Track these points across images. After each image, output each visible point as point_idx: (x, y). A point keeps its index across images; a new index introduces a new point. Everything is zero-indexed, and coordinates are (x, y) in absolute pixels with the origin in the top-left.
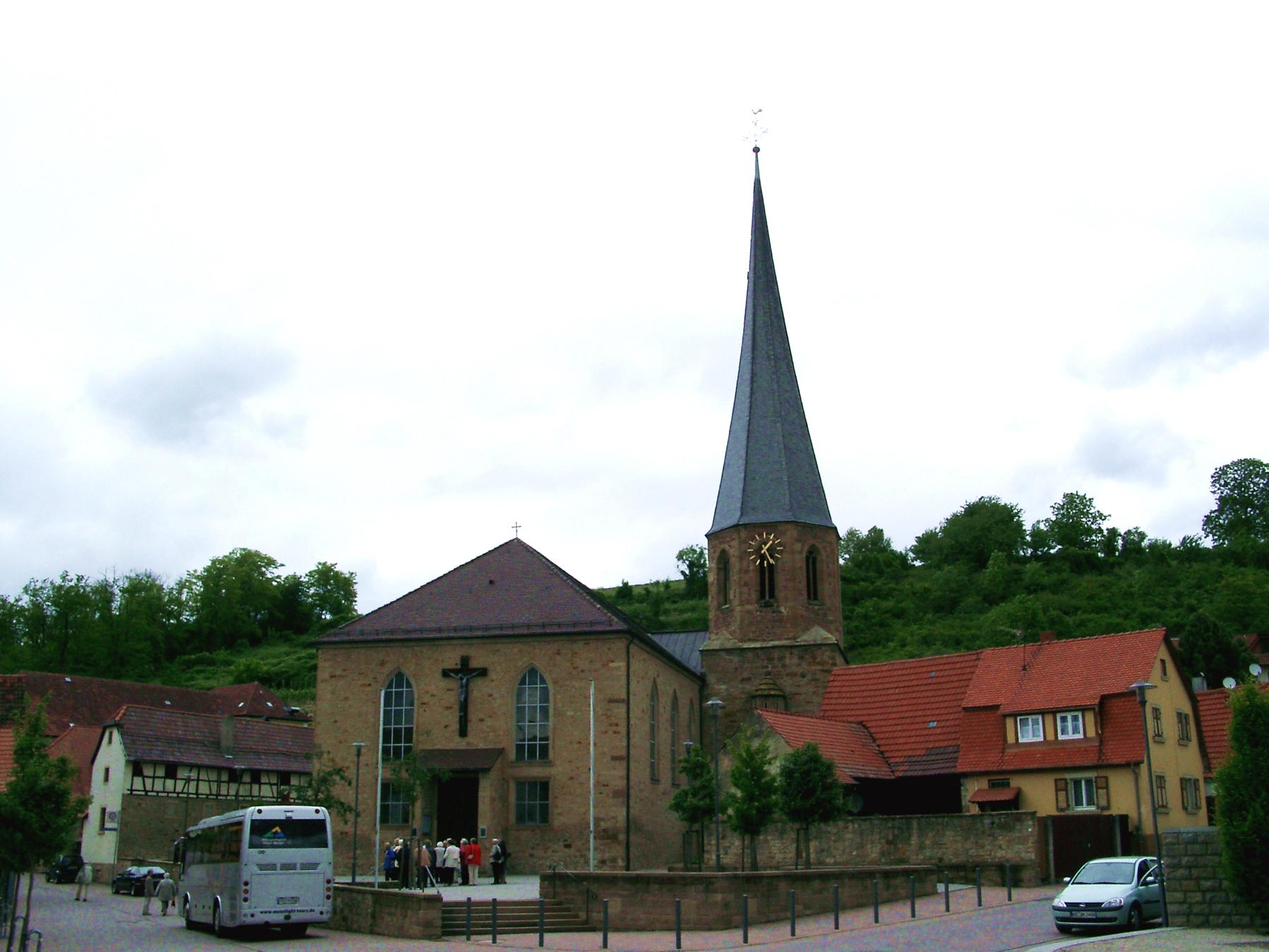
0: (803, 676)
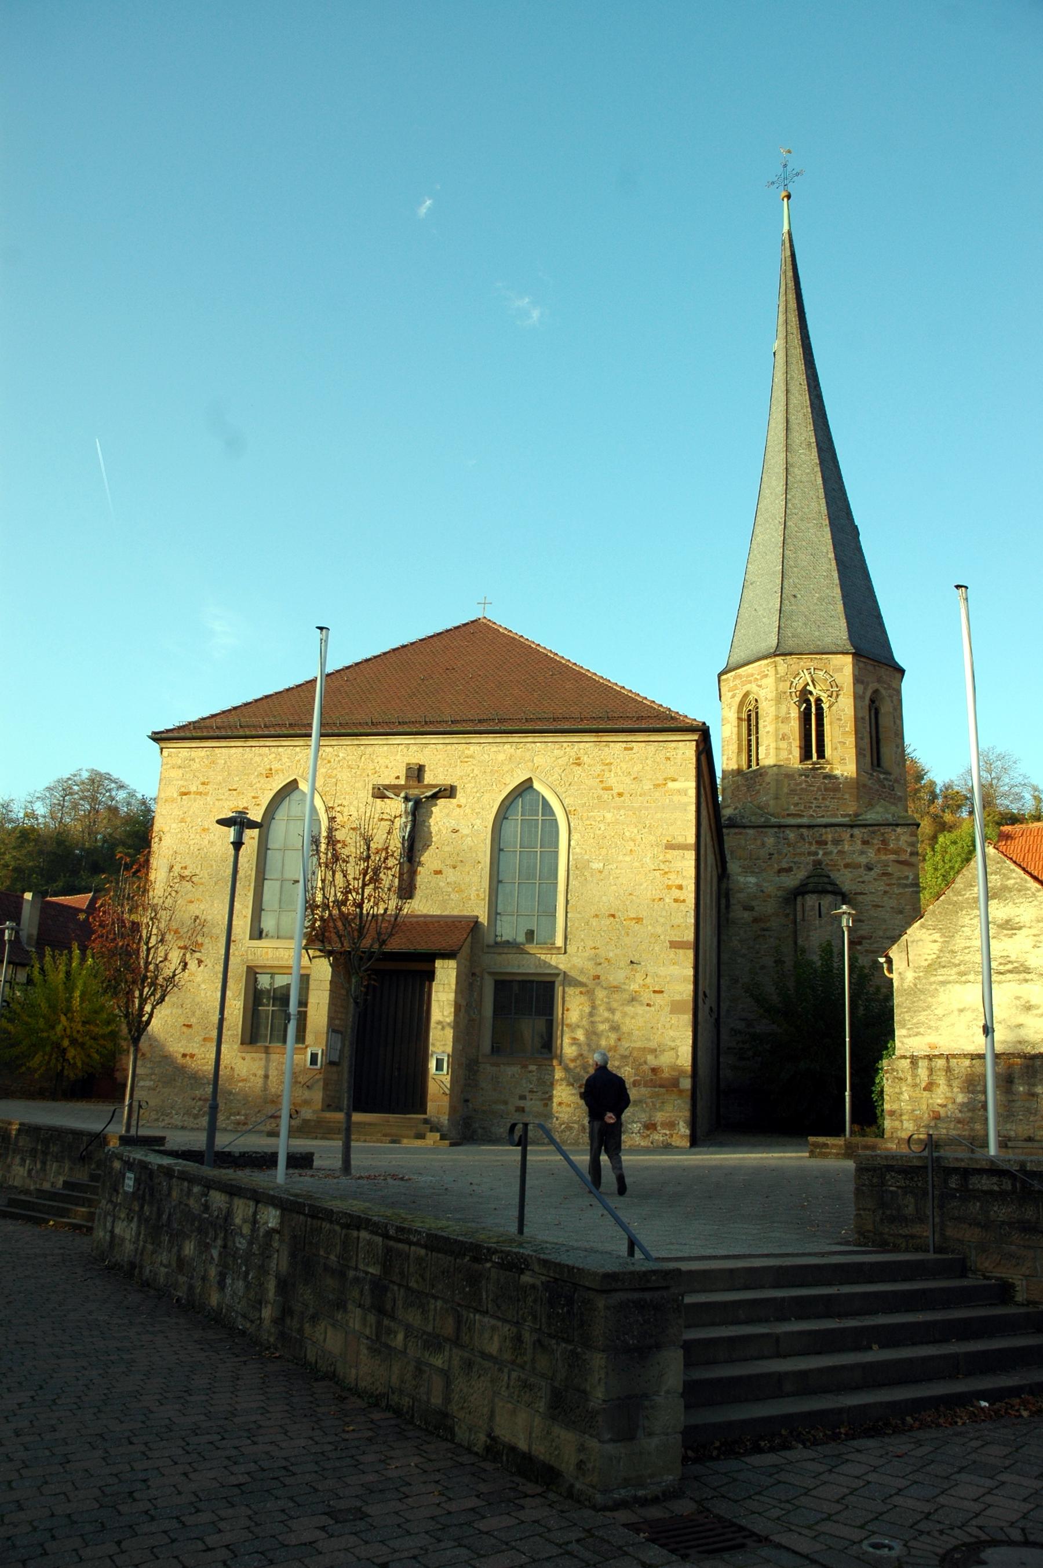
0: (869, 868)
